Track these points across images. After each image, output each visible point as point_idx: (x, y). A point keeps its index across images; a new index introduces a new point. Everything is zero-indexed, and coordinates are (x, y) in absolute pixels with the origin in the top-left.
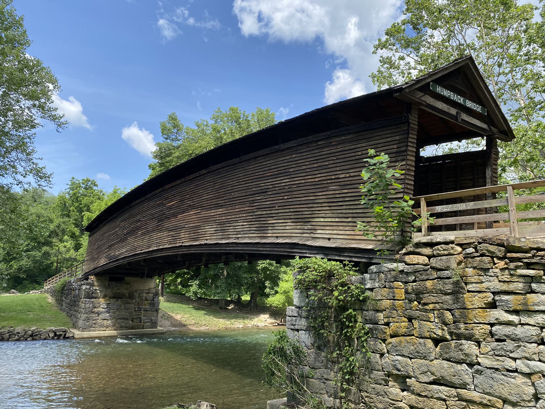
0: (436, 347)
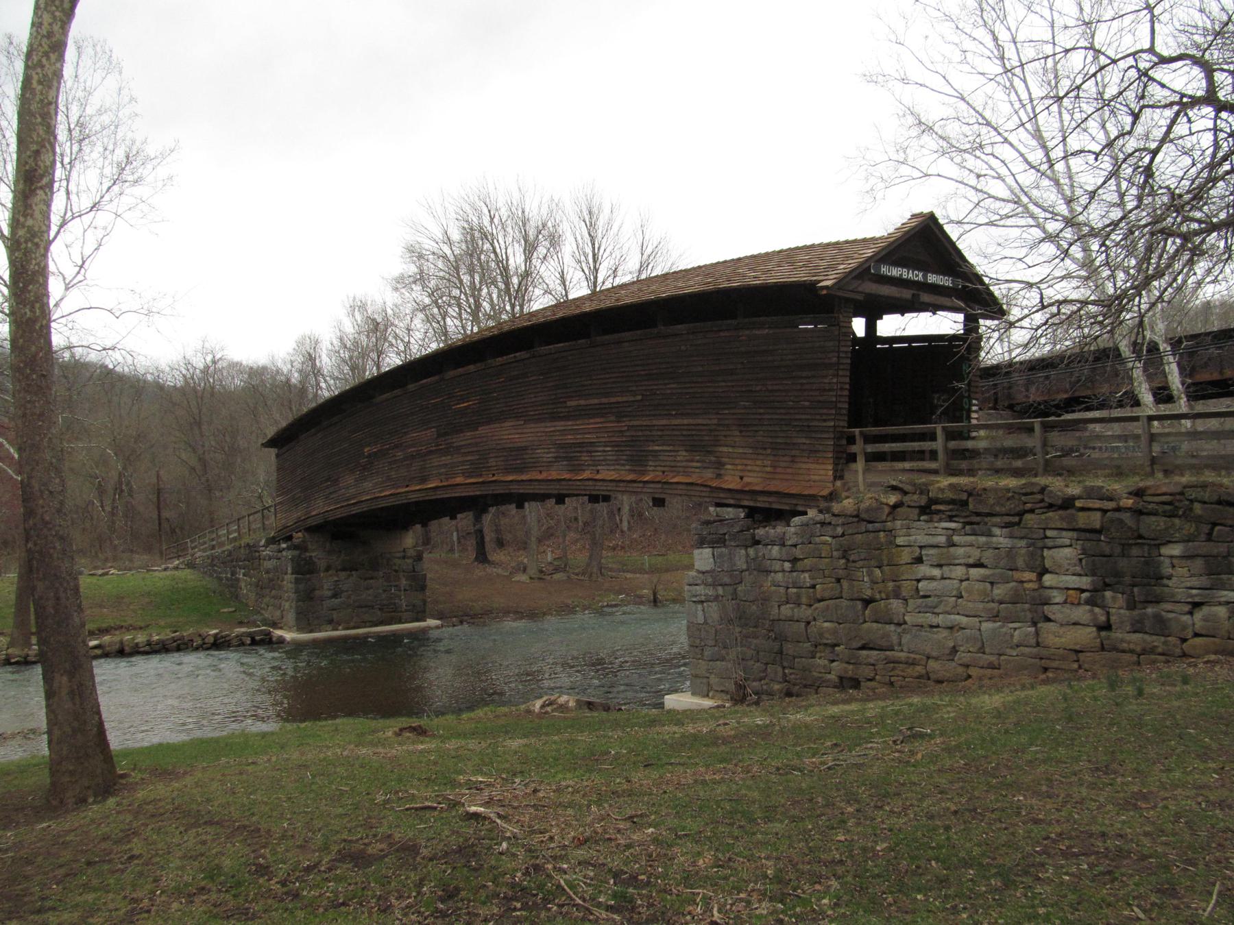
0: (866, 607)
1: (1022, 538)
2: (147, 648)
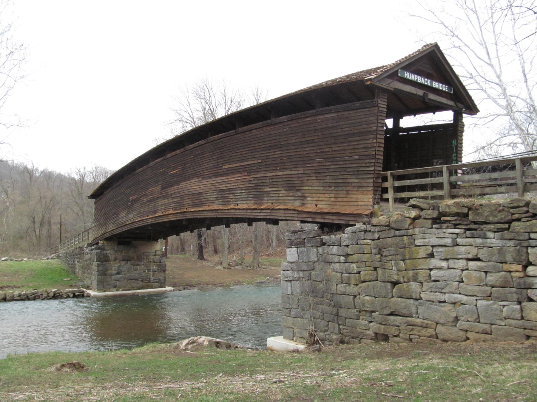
1: (511, 239)
2: (19, 298)
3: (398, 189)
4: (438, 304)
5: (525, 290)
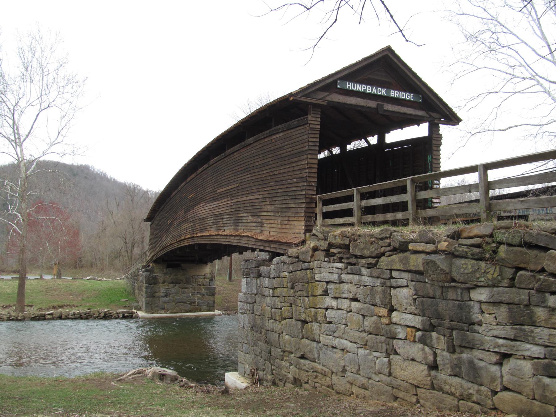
2: (73, 317)
3: (327, 216)
4: (331, 349)
5: (391, 340)
